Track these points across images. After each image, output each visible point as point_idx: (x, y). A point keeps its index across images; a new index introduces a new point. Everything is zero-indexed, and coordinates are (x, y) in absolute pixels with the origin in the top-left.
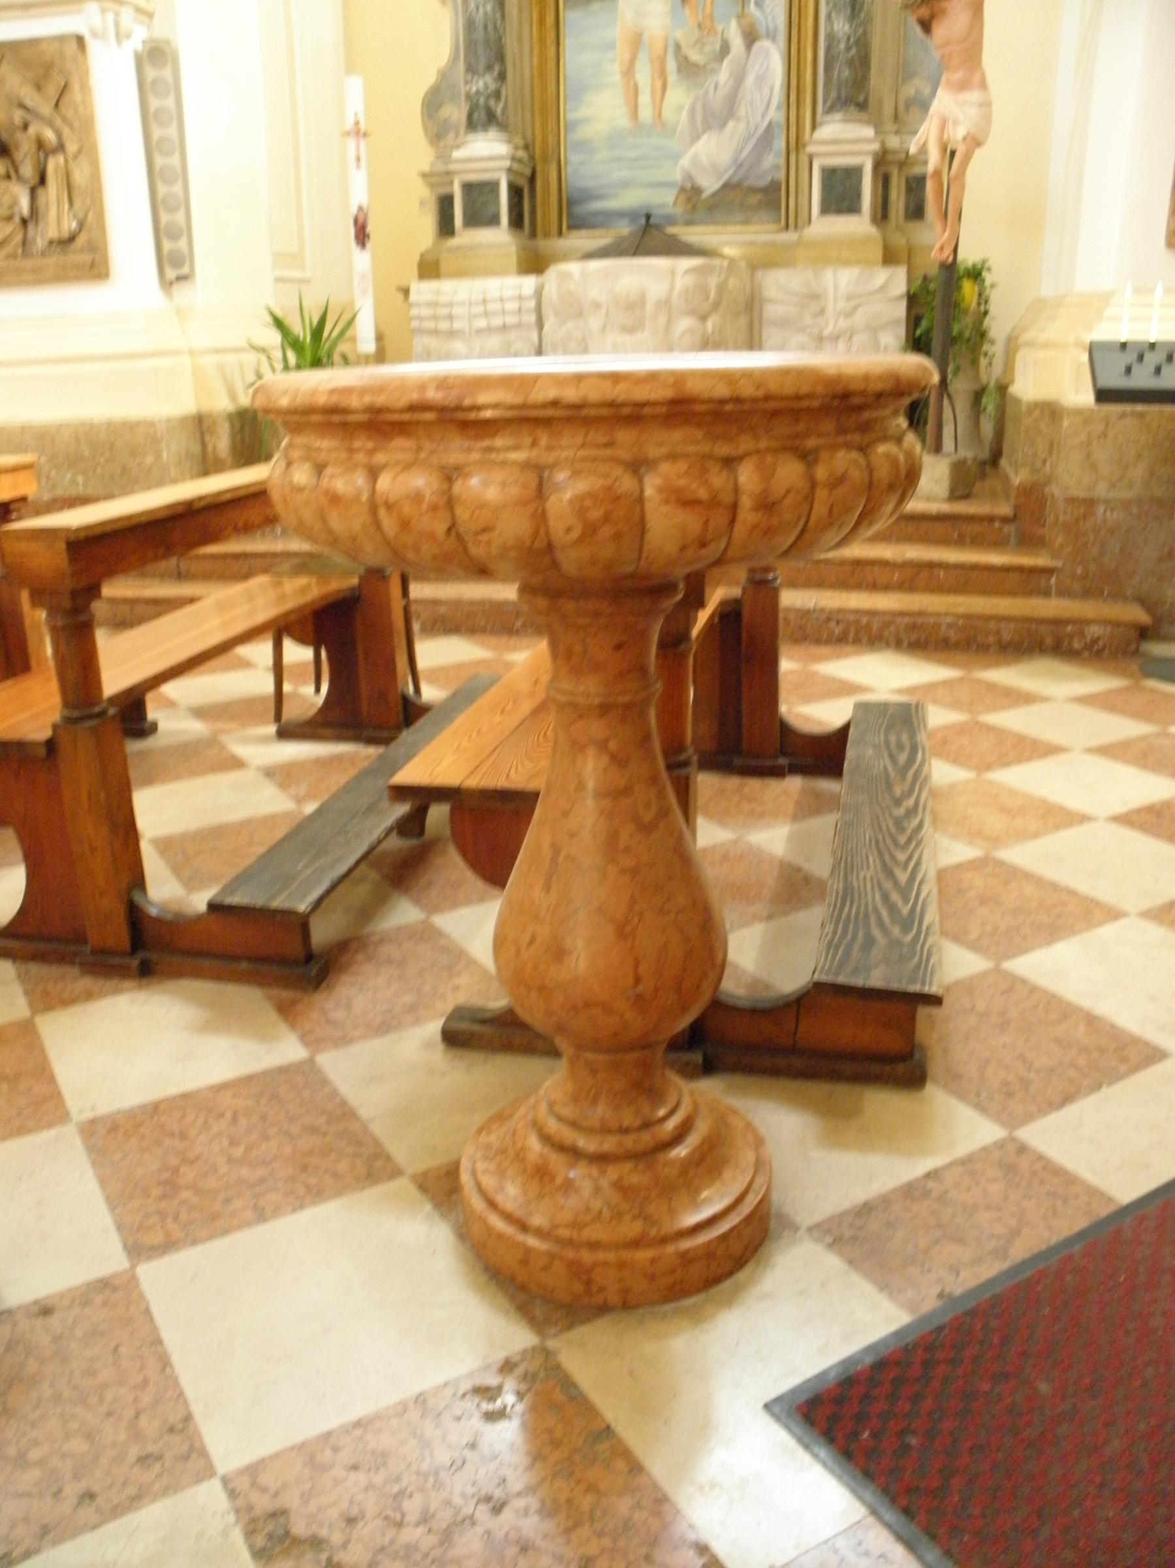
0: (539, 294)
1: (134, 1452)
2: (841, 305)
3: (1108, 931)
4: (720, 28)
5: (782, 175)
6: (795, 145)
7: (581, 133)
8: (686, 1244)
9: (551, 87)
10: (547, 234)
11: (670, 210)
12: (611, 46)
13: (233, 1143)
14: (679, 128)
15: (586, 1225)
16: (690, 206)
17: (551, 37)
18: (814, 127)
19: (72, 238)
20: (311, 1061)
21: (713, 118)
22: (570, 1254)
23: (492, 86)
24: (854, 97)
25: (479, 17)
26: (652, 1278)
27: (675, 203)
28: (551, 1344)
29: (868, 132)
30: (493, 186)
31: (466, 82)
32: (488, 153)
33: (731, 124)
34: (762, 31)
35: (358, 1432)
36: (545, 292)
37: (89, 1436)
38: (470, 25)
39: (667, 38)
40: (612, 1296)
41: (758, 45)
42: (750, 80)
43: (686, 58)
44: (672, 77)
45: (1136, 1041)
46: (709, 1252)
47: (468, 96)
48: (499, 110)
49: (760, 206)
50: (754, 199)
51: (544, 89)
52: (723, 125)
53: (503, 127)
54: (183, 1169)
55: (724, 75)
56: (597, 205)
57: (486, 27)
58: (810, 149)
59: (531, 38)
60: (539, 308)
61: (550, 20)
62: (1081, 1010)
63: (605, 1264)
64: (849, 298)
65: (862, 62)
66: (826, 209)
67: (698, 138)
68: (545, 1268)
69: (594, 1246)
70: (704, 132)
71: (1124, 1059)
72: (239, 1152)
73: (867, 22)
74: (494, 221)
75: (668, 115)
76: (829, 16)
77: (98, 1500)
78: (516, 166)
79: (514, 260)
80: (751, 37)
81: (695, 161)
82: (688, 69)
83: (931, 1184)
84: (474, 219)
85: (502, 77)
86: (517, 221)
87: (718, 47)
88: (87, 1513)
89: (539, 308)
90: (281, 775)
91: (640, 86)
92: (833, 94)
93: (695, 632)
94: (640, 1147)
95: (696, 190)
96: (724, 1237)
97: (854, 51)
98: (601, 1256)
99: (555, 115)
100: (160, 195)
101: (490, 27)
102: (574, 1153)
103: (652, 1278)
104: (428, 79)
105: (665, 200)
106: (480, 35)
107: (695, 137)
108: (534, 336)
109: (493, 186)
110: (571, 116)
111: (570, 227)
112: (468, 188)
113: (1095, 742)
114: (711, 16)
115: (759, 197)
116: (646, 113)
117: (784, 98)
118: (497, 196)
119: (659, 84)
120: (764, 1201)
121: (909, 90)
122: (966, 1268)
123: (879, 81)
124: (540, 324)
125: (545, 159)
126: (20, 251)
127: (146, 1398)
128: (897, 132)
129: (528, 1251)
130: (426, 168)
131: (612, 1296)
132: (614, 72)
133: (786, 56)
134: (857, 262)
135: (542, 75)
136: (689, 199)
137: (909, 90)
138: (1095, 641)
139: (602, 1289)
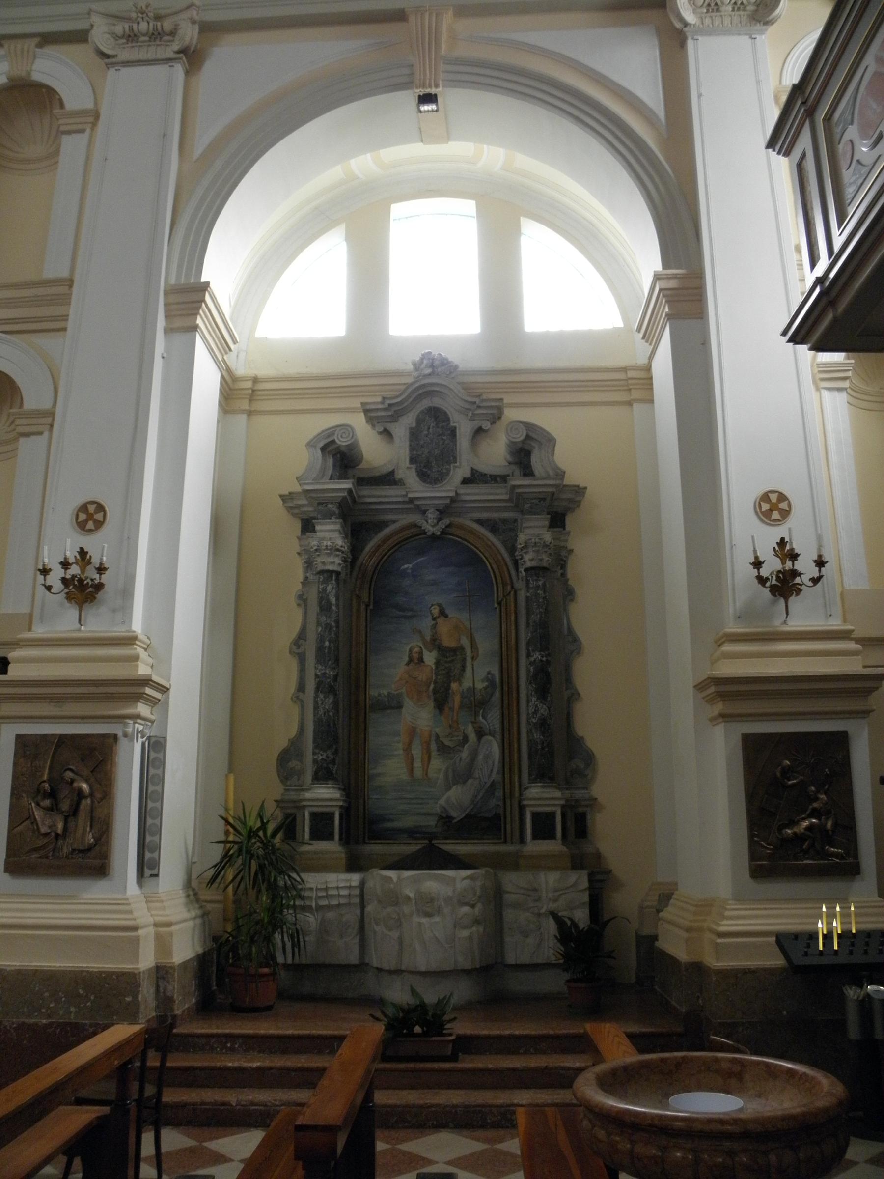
0: (362, 884)
2: (550, 895)
19: (90, 849)
21: (460, 777)
24: (544, 774)
29: (558, 794)
31: (314, 753)
32: (326, 795)
33: (470, 781)
36: (367, 885)
39: (431, 731)
42: (481, 757)
44: (434, 753)
47: (315, 761)
52: (465, 782)
53: (335, 780)
55: (465, 754)
56: (389, 825)
60: (362, 895)
64: (556, 890)
66: (535, 837)
70: (454, 785)
74: (330, 837)
75: (432, 774)
79: (344, 862)
80: (480, 734)
82: (443, 749)
84: (317, 835)
89: (362, 895)
93: (339, 1151)
100: (148, 824)
104: (281, 742)
107: (449, 788)
108: (358, 912)
112: (314, 815)
116: (418, 773)
118: (333, 822)
124: (363, 906)
126: (50, 854)
128: (567, 789)
130: (278, 798)
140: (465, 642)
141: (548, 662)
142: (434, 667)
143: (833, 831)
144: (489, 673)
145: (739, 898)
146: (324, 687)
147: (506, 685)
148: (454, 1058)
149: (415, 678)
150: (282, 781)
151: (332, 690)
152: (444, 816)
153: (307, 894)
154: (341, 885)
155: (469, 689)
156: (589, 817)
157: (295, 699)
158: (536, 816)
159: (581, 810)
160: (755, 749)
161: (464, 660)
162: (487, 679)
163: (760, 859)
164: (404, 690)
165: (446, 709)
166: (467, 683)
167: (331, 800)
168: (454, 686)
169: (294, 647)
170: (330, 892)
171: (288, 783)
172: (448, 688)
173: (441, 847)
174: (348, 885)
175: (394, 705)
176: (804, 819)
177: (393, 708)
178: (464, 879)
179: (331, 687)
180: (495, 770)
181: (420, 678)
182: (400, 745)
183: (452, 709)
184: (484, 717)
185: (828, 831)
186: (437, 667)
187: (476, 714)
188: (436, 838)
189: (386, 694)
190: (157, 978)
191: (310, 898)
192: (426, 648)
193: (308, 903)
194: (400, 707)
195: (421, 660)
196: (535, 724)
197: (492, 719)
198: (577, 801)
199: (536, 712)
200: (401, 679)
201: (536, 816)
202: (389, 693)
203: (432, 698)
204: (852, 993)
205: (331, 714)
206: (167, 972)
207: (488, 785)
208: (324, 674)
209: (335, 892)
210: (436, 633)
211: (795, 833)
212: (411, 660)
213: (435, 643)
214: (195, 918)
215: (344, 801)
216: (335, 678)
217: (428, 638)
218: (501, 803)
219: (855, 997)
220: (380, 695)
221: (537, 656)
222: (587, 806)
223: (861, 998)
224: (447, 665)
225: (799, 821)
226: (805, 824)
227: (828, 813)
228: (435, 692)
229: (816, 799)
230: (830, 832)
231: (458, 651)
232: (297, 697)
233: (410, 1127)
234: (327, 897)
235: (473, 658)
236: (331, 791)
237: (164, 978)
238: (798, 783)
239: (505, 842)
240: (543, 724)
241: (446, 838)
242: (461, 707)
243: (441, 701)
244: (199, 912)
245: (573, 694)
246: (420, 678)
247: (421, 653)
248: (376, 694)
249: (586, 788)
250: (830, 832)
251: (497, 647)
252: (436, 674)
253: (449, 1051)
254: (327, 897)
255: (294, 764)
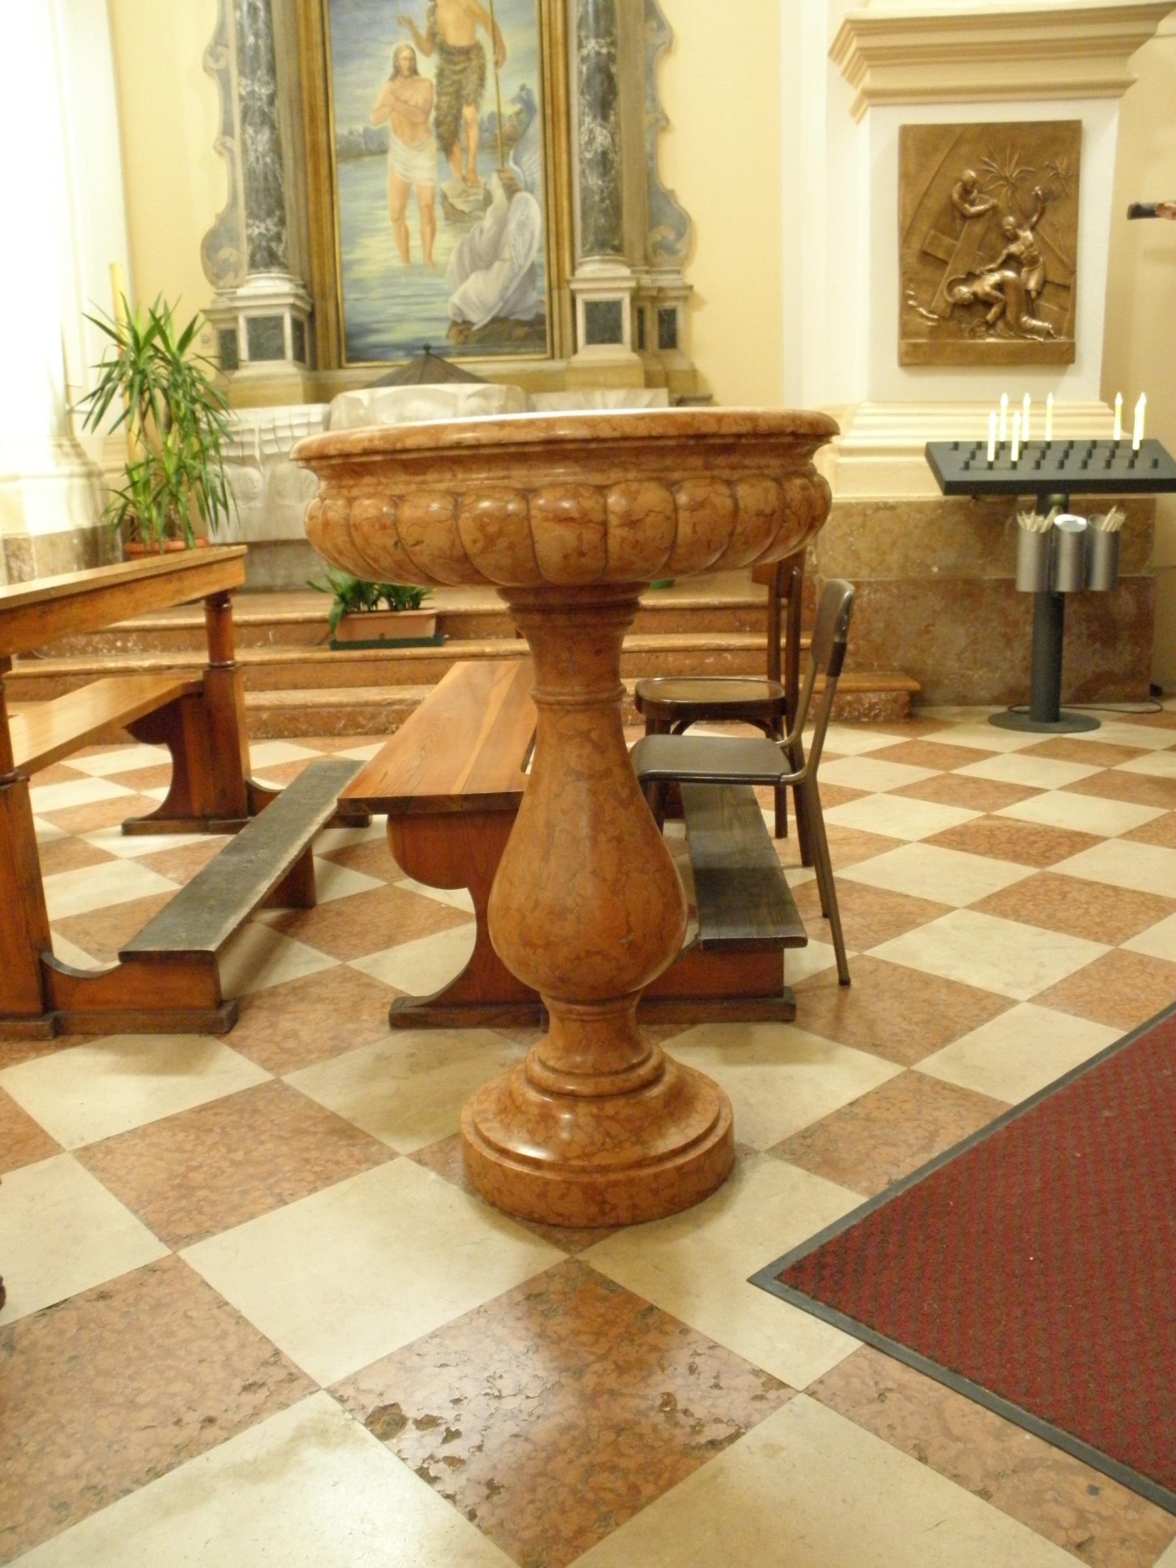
1: (238, 1384)
3: (943, 921)
4: (482, 180)
5: (546, 312)
6: (558, 282)
7: (359, 272)
8: (680, 1161)
9: (327, 232)
10: (328, 367)
11: (444, 343)
12: (382, 196)
13: (231, 1150)
14: (449, 267)
15: (593, 1155)
16: (461, 338)
17: (325, 186)
18: (573, 269)
20: (278, 1081)
21: (482, 259)
22: (585, 1179)
23: (274, 229)
24: (608, 242)
25: (259, 168)
26: (655, 1192)
27: (447, 336)
28: (581, 1257)
29: (625, 271)
30: (277, 322)
31: (248, 226)
32: (271, 290)
33: (497, 265)
34: (521, 185)
35: (436, 1341)
37: (190, 1379)
38: (250, 175)
39: (433, 188)
40: (624, 1214)
41: (518, 196)
42: (512, 226)
43: (452, 206)
44: (440, 223)
45: (989, 995)
46: (697, 1167)
47: (250, 239)
48: (280, 253)
49: (526, 337)
50: (520, 332)
51: (320, 233)
52: (488, 266)
53: (284, 267)
54: (191, 1175)
55: (488, 221)
57: (266, 178)
58: (574, 286)
59: (306, 184)
61: (324, 171)
62: (939, 978)
63: (615, 1184)
65: (614, 211)
66: (591, 339)
67: (467, 277)
68: (563, 1197)
69: (604, 1169)
70: (473, 271)
71: (984, 1009)
72: (239, 1156)
73: (617, 179)
74: (279, 354)
75: (438, 256)
76: (583, 172)
77: (219, 1422)
78: (299, 303)
79: (301, 389)
80: (511, 190)
81: (464, 298)
82: (455, 216)
83: (855, 1110)
84: (258, 353)
85: (282, 222)
86: (299, 356)
87: (481, 197)
88: (211, 1433)
90: (156, 862)
91: (411, 230)
92: (591, 238)
94: (629, 1085)
95: (467, 324)
96: (709, 1153)
97: (608, 202)
98: (612, 1177)
99: (330, 254)
101: (270, 178)
102: (572, 1099)
103: (655, 1192)
104: (206, 222)
105: (439, 333)
106: (260, 184)
107: (464, 277)
109: (277, 322)
110: (347, 257)
111: (350, 360)
112: (252, 322)
113: (892, 786)
114: (474, 171)
115: (526, 329)
116: (417, 255)
117: (544, 244)
119: (428, 229)
120: (726, 1139)
121: (656, 236)
122: (905, 1159)
123: (630, 229)
125: (323, 296)
127: (231, 1345)
128: (647, 272)
129: (547, 1183)
131: (624, 1214)
132: (385, 217)
133: (544, 206)
134: (621, 386)
135: (318, 220)
136: (461, 332)
137: (656, 236)
138: (872, 707)
139: (614, 1208)
140: (483, 36)
141: (611, 58)
142: (434, 81)
143: (1039, 293)
144: (523, 88)
145: (878, 398)
146: (258, 115)
147: (551, 110)
148: (436, 641)
149: (406, 102)
150: (212, 283)
151: (267, 121)
152: (459, 320)
153: (246, 438)
154: (294, 422)
155: (492, 116)
156: (680, 317)
157: (219, 148)
158: (591, 307)
159: (668, 305)
160: (922, 148)
161: (482, 68)
162: (519, 99)
163: (917, 334)
164: (388, 124)
165: (456, 149)
166: (488, 107)
167: (276, 295)
168: (468, 112)
169: (210, 61)
170: (280, 434)
171: (221, 283)
172: (458, 117)
173: (460, 366)
174: (305, 421)
175: (373, 148)
176: (991, 271)
177: (371, 153)
178: (470, 396)
179: (263, 114)
180: (536, 246)
181: (412, 102)
182: (387, 214)
183: (465, 150)
184: (516, 162)
185: (1028, 292)
186: (440, 82)
187: (504, 158)
188: (448, 355)
189: (361, 130)
190: (7, 556)
191: (251, 445)
192: (422, 50)
193: (247, 452)
194: (383, 151)
195: (414, 71)
196: (591, 160)
197: (529, 164)
198: (660, 289)
199: (591, 140)
200: (383, 105)
201: (591, 307)
202: (366, 130)
203: (434, 134)
204: (1031, 524)
205: (268, 160)
206: (20, 548)
207: (525, 269)
208: (252, 93)
209: (286, 433)
210: (435, 23)
211: (975, 294)
212: (397, 71)
213: (435, 40)
214: (71, 476)
215: (296, 296)
216: (272, 99)
217: (423, 32)
218: (545, 298)
219: (1034, 529)
220: (351, 133)
221: (592, 45)
222: (677, 298)
223: (1043, 530)
224: (455, 78)
225: (982, 273)
226: (995, 278)
227: (1033, 262)
228: (438, 123)
229: (1015, 238)
230: (1034, 294)
231: (471, 52)
232: (223, 144)
233: (366, 734)
234: (277, 441)
235: (497, 64)
236: (278, 283)
237: (16, 557)
238: (986, 211)
239: (553, 357)
240: (604, 163)
241: (463, 354)
242: (481, 146)
243: (448, 139)
244: (79, 469)
245: (657, 120)
246: (412, 102)
247: (413, 59)
248: (346, 133)
249: (678, 272)
250: (1034, 294)
251: (535, 43)
252: (439, 95)
253: (430, 630)
254: (277, 441)
255: (226, 253)
